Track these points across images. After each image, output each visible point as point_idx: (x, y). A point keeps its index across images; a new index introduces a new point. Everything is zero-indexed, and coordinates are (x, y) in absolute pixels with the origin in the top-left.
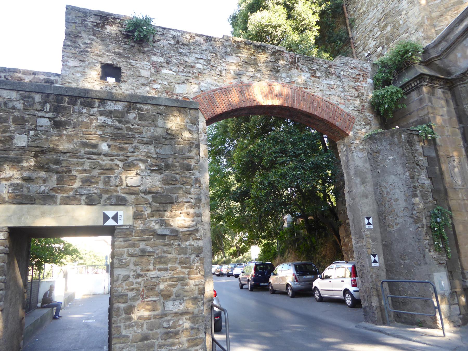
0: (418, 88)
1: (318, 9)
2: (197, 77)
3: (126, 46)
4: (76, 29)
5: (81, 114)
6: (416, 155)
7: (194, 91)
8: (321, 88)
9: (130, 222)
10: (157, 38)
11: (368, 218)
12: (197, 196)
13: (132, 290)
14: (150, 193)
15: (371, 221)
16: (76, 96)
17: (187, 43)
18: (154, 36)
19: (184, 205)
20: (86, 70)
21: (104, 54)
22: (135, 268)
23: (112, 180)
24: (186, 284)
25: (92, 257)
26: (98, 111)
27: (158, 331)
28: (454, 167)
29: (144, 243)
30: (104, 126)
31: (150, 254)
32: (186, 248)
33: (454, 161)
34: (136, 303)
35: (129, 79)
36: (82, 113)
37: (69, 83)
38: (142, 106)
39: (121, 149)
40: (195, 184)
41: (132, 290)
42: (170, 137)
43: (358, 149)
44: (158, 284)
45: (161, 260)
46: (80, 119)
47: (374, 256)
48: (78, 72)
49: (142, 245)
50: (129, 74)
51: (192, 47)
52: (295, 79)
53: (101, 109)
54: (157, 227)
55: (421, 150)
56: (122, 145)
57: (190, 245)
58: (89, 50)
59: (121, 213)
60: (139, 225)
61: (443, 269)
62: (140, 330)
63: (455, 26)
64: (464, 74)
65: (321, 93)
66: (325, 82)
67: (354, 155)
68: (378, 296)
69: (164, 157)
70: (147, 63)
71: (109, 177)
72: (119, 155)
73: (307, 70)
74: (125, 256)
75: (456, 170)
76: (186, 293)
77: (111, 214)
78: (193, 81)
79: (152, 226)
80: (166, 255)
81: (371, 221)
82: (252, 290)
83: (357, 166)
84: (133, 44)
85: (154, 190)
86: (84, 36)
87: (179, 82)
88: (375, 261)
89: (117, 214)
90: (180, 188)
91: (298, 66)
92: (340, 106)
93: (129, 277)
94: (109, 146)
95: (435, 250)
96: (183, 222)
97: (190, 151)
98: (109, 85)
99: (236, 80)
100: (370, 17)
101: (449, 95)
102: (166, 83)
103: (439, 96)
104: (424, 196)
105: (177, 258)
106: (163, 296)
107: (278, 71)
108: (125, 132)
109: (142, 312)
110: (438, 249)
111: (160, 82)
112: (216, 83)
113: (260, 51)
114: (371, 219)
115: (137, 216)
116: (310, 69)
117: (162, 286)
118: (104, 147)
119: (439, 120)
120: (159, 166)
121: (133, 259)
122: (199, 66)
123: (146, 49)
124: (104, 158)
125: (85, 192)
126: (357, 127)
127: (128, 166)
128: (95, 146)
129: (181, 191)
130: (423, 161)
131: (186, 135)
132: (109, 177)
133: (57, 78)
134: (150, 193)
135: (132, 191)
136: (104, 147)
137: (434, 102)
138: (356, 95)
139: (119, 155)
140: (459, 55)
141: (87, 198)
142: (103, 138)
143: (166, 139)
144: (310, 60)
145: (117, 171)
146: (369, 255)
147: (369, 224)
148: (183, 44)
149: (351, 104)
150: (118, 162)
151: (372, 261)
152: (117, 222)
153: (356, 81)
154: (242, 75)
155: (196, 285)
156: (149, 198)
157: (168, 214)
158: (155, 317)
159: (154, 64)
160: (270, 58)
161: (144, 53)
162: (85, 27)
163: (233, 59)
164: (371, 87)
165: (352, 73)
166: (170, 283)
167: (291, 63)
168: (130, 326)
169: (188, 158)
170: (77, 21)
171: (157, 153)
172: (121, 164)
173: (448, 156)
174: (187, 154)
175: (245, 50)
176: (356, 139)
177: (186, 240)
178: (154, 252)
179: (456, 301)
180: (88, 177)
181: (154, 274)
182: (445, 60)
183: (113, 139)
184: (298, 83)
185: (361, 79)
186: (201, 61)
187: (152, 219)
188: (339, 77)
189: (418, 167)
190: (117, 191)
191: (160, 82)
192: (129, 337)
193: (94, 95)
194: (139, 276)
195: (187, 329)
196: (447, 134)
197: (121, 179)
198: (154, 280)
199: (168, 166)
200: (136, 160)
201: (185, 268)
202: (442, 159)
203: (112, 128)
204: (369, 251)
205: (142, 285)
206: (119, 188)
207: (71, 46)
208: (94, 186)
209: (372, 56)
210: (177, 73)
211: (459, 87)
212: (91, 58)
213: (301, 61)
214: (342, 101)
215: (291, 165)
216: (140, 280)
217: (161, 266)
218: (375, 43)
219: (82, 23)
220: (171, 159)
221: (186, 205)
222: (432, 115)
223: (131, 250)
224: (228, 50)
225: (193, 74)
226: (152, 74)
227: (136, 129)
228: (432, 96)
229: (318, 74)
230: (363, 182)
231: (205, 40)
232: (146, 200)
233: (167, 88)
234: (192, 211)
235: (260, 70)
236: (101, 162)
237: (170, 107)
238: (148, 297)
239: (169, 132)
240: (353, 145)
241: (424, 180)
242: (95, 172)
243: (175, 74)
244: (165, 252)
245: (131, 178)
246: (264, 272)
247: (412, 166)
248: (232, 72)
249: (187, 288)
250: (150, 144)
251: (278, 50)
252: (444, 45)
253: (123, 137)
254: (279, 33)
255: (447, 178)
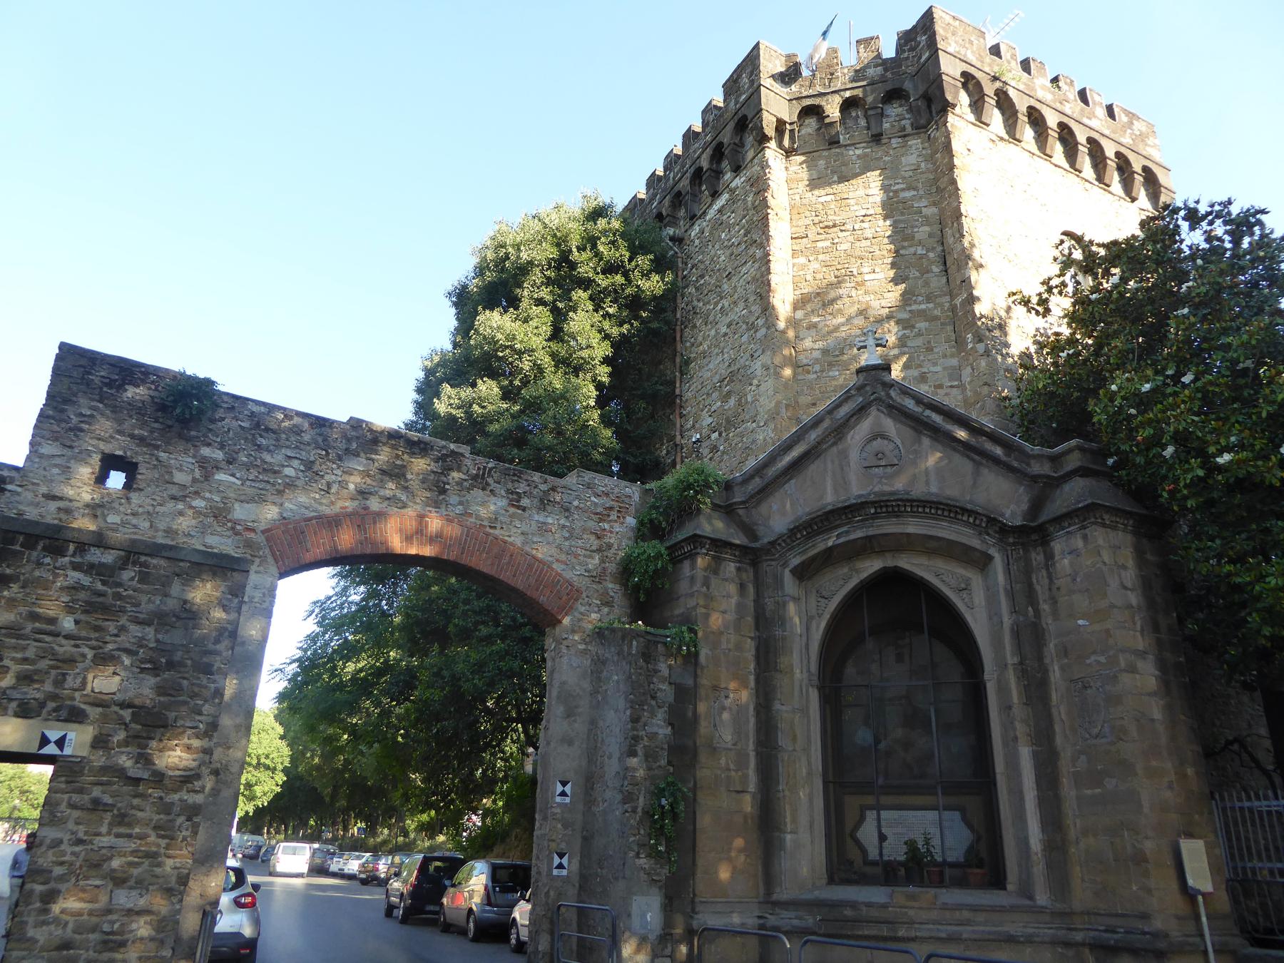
0: (692, 556)
1: (615, 331)
2: (280, 493)
3: (156, 425)
4: (69, 388)
5: (39, 564)
6: (655, 680)
7: (269, 516)
8: (525, 528)
9: (84, 752)
10: (220, 413)
11: (564, 784)
12: (210, 719)
13: (62, 863)
14: (130, 706)
15: (568, 789)
16: (37, 536)
17: (274, 427)
18: (214, 411)
19: (184, 732)
20: (72, 464)
21: (112, 437)
22: (75, 828)
23: (69, 679)
24: (159, 865)
25: (17, 792)
26: (71, 562)
27: (91, 936)
28: (724, 708)
29: (100, 788)
30: (75, 588)
31: (107, 808)
32: (173, 804)
33: (727, 697)
34: (63, 887)
35: (149, 486)
36: (42, 564)
37: (34, 484)
38: (149, 559)
39: (97, 629)
40: (214, 697)
41: (62, 863)
42: (189, 615)
43: (573, 651)
44: (110, 858)
45: (122, 819)
46: (37, 573)
47: (561, 856)
48: (56, 466)
49: (96, 792)
50: (150, 476)
51: (284, 436)
52: (474, 508)
53: (78, 559)
54: (129, 764)
55: (665, 672)
56: (100, 623)
57: (180, 800)
58: (85, 426)
59: (71, 736)
60: (99, 759)
61: (655, 890)
62: (60, 932)
63: (779, 455)
64: (772, 543)
65: (522, 538)
66: (536, 517)
67: (567, 662)
68: (552, 933)
69: (168, 648)
70: (190, 460)
71: (64, 675)
72: (90, 639)
73: (503, 493)
74: (63, 807)
75: (726, 716)
76: (154, 880)
77: (53, 735)
78: (271, 498)
79: (120, 762)
80: (133, 812)
81: (568, 789)
82: (404, 920)
83: (564, 683)
84: (170, 423)
85: (137, 702)
86: (83, 401)
87: (243, 498)
88: (560, 866)
89: (64, 738)
90: (185, 703)
91: (488, 484)
92: (554, 566)
93: (61, 842)
94: (77, 622)
95: (649, 856)
96: (176, 760)
97: (217, 641)
98: (109, 494)
99: (356, 503)
100: (711, 366)
101: (749, 575)
102: (217, 499)
103: (728, 575)
104: (650, 756)
105: (151, 820)
106: (113, 879)
107: (443, 491)
108: (109, 600)
109: (70, 903)
110: (654, 854)
111: (207, 495)
112: (316, 505)
113: (417, 451)
114: (569, 786)
115: (100, 742)
116: (509, 492)
117: (116, 863)
118: (68, 624)
119: (716, 621)
120: (158, 662)
121: (76, 814)
122: (289, 471)
123: (193, 433)
124: (64, 642)
125: (18, 696)
126: (582, 609)
127: (103, 659)
128: (53, 621)
129: (183, 709)
130: (666, 691)
131: (218, 614)
132: (64, 675)
133: (13, 474)
134: (130, 706)
135: (100, 702)
136: (68, 624)
137: (713, 586)
138: (594, 548)
139: (90, 639)
140: (775, 507)
141: (19, 706)
142: (69, 609)
143: (178, 618)
144: (514, 475)
145: (81, 665)
146: (551, 853)
147: (563, 794)
148: (267, 430)
149: (580, 564)
150: (86, 650)
151: (556, 864)
152: (62, 750)
153: (601, 520)
154: (370, 493)
155: (176, 868)
156: (127, 714)
157: (154, 744)
158: (91, 913)
159: (203, 463)
160: (433, 467)
161: (188, 440)
162: (88, 385)
163: (358, 464)
164: (631, 534)
165: (596, 504)
166: (130, 859)
167: (475, 477)
168: (44, 923)
169: (211, 653)
170: (75, 374)
171: (157, 641)
172: (90, 654)
173: (715, 688)
174: (211, 647)
175: (386, 449)
176: (573, 631)
177: (175, 791)
178: (113, 806)
179: (668, 951)
180: (27, 670)
181: (106, 841)
182: (754, 511)
183: (86, 612)
184: (478, 517)
185: (614, 516)
186: (296, 463)
187: (123, 749)
188: (567, 510)
189: (653, 703)
190: (73, 699)
191: (207, 495)
192: (37, 941)
193: (69, 535)
194: (80, 842)
195: (142, 939)
196: (724, 646)
197: (85, 678)
198: (104, 851)
199: (171, 665)
200: (118, 649)
201: (163, 837)
202: (702, 692)
203: (89, 593)
204: (553, 845)
205: (81, 858)
206: (77, 695)
207: (53, 418)
208: (36, 686)
209: (704, 445)
210: (244, 481)
211: (765, 564)
212: (89, 443)
213: (496, 476)
214: (563, 557)
215: (499, 645)
216: (77, 849)
217: (122, 830)
218: (710, 420)
219: (83, 378)
220: (180, 653)
221: (189, 732)
222: (703, 610)
223: (76, 798)
224: (354, 446)
225: (274, 485)
226: (194, 480)
227: (129, 597)
228: (712, 576)
229: (525, 502)
230: (570, 714)
231: (311, 424)
232: (121, 718)
233: (218, 508)
234: (196, 743)
235: (407, 488)
236: (57, 648)
237: (198, 564)
238: (86, 878)
239: (187, 607)
240: (565, 642)
241: (659, 727)
242: (43, 664)
243: (239, 482)
244: (133, 807)
245: (105, 682)
246: (436, 879)
247: (641, 697)
248: (352, 486)
249: (158, 870)
250: (149, 625)
251: (453, 451)
252: (757, 483)
253: (105, 609)
254: (526, 365)
255: (704, 728)
